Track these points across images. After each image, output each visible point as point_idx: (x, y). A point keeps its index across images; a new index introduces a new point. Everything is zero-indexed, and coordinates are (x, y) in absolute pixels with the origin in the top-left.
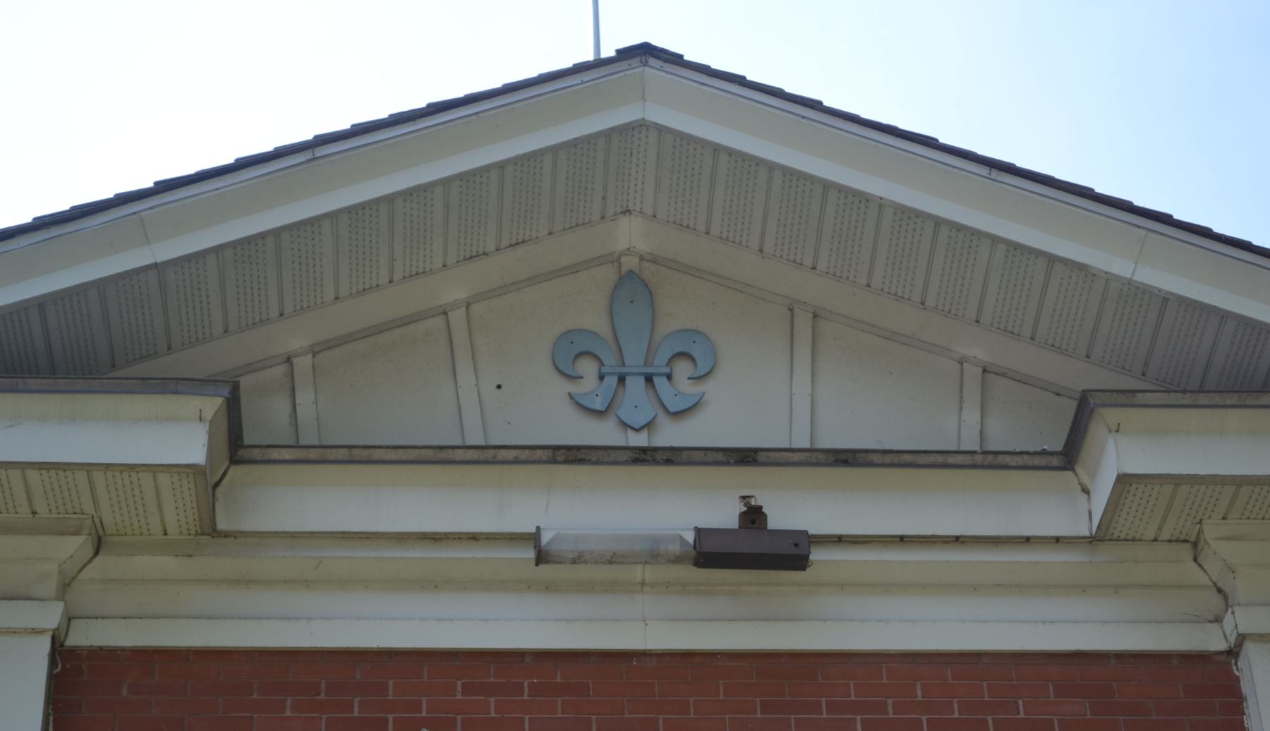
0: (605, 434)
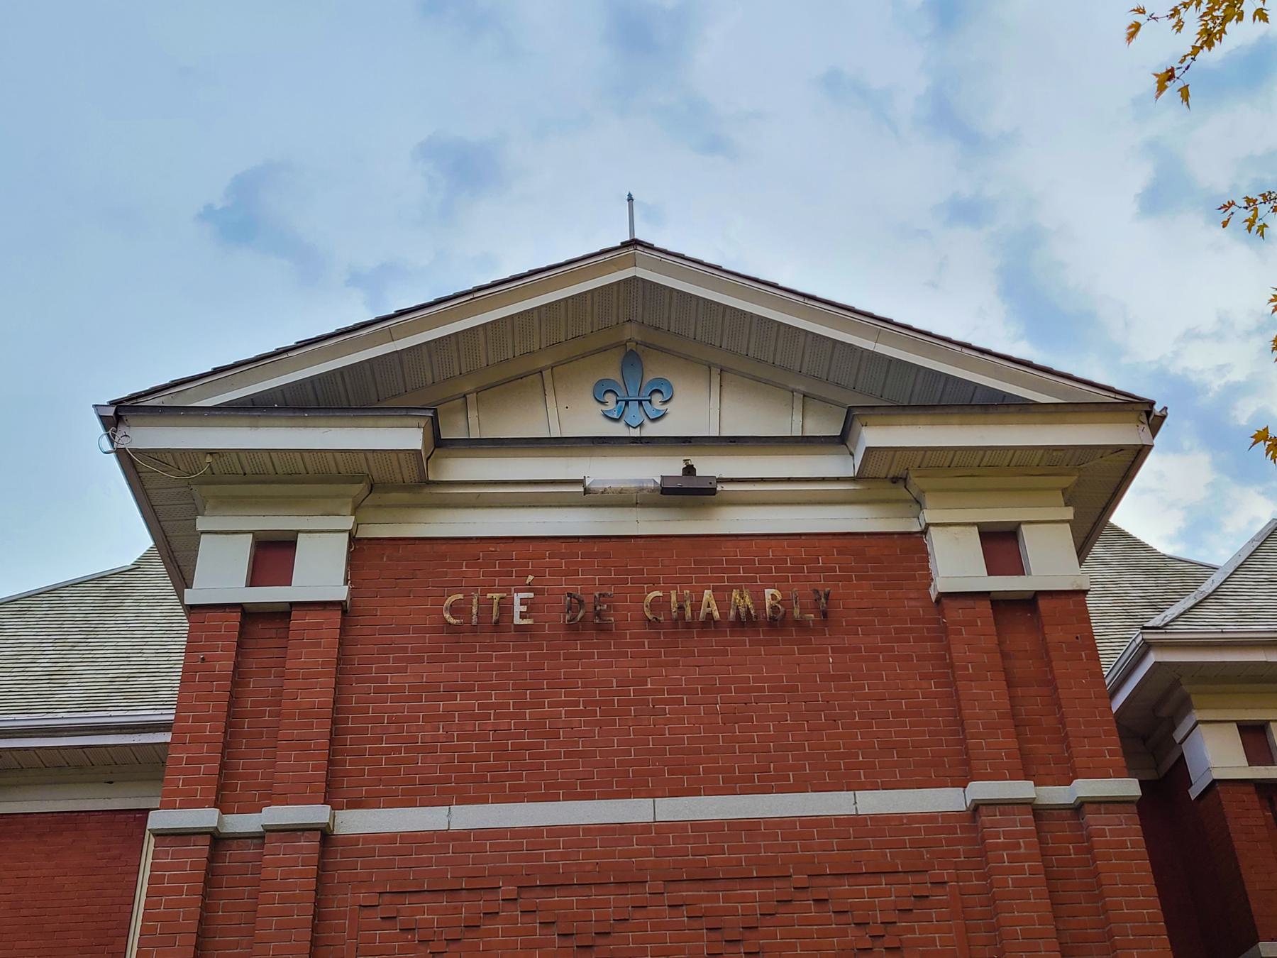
0: (619, 430)
